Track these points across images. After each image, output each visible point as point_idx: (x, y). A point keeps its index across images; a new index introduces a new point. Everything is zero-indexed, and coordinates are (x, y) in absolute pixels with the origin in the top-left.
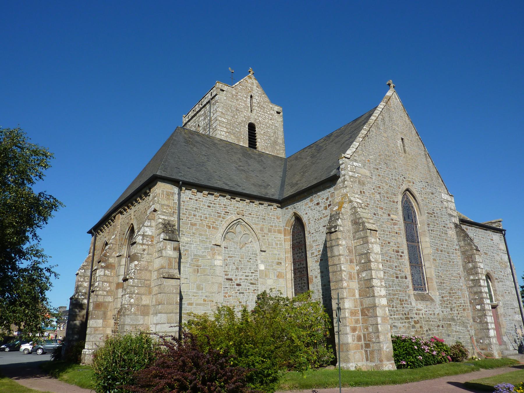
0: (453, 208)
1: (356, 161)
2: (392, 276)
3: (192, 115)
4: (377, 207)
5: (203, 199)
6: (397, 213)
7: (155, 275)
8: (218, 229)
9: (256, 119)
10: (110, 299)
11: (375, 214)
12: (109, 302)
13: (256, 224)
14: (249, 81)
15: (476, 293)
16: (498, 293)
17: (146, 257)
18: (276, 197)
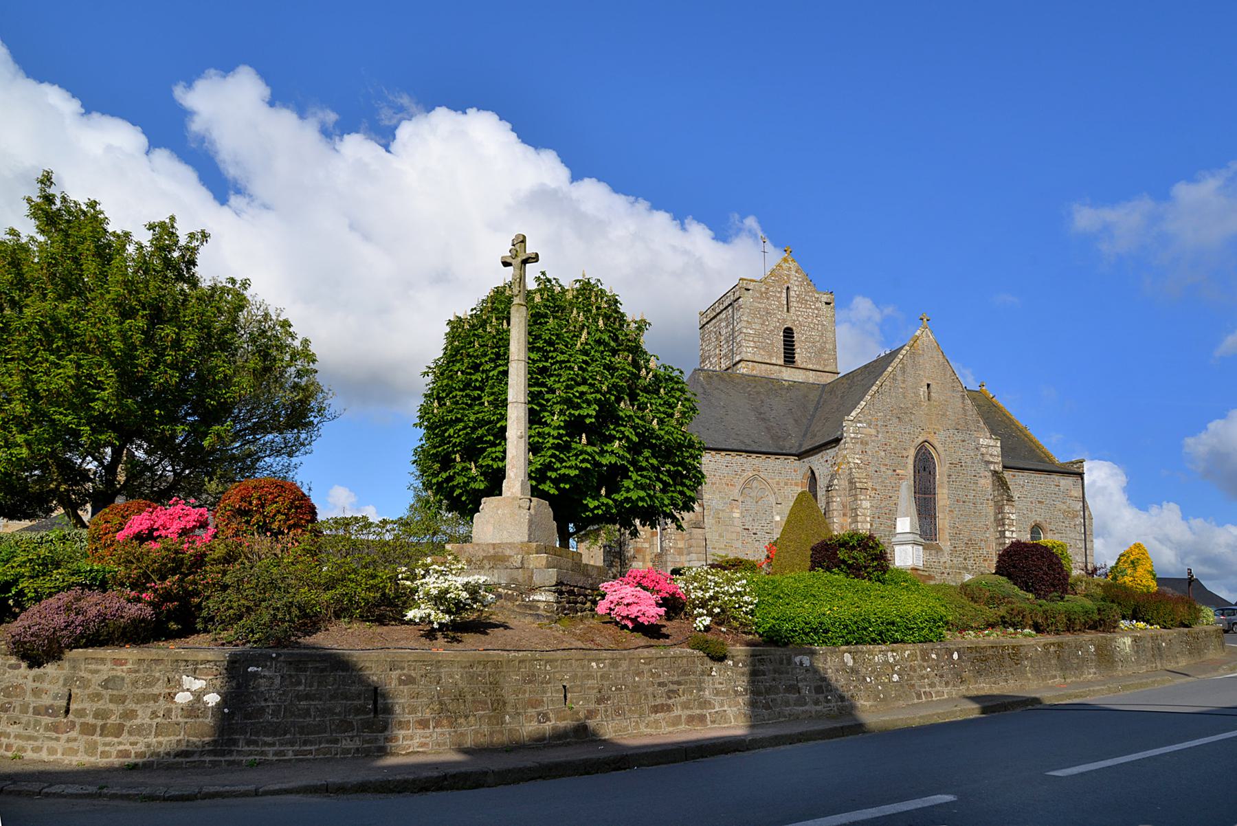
1: (860, 422)
6: (905, 466)
10: (647, 545)
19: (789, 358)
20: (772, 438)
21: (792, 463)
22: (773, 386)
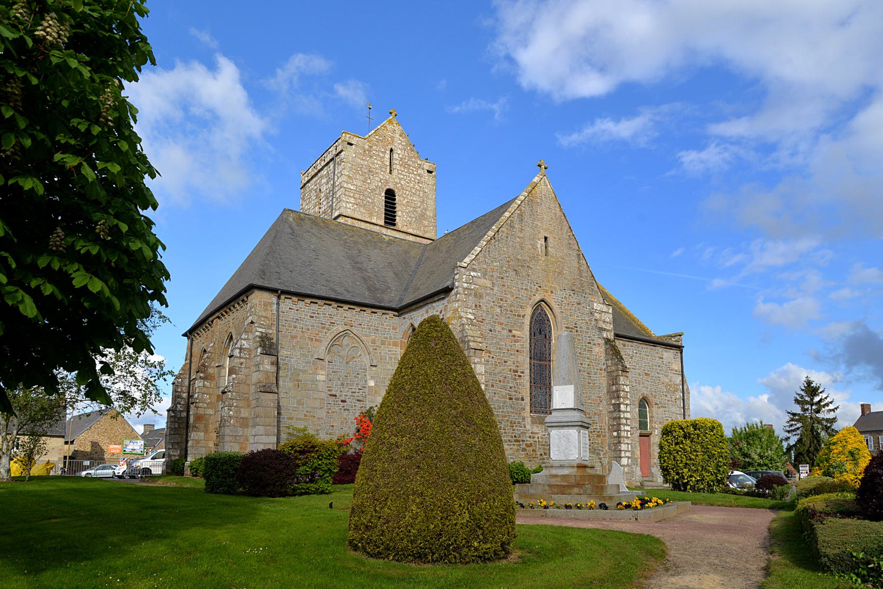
0: (608, 320)
1: (474, 270)
2: (504, 397)
3: (313, 173)
4: (495, 322)
5: (305, 308)
6: (521, 328)
7: (253, 389)
8: (321, 342)
9: (397, 183)
10: (211, 411)
11: (491, 331)
12: (211, 415)
13: (366, 336)
14: (390, 127)
15: (615, 418)
16: (655, 420)
17: (244, 371)
18: (393, 305)
19: (390, 219)
20: (369, 289)
21: (389, 320)
22: (373, 240)
